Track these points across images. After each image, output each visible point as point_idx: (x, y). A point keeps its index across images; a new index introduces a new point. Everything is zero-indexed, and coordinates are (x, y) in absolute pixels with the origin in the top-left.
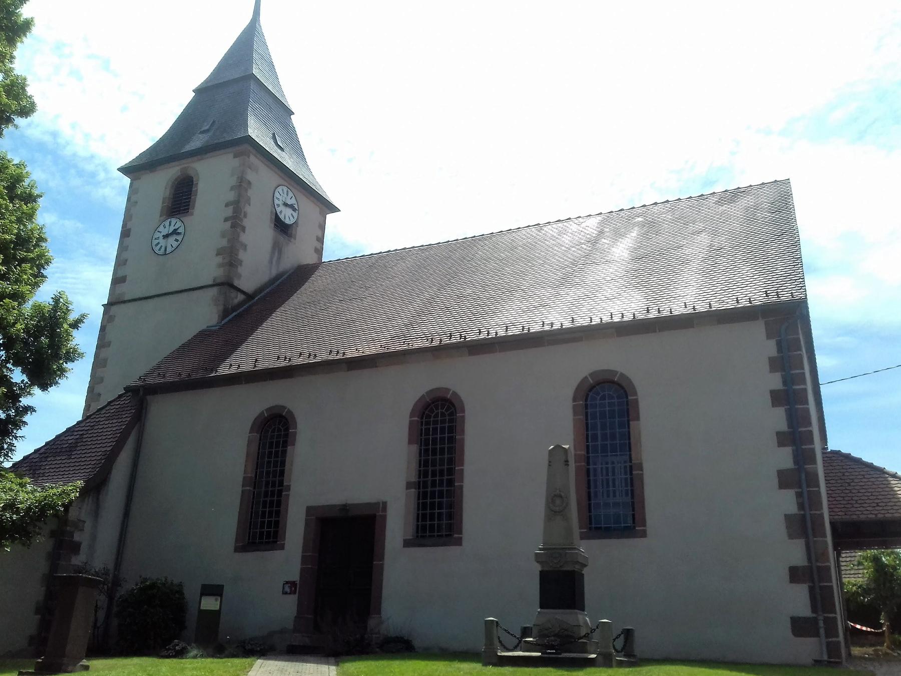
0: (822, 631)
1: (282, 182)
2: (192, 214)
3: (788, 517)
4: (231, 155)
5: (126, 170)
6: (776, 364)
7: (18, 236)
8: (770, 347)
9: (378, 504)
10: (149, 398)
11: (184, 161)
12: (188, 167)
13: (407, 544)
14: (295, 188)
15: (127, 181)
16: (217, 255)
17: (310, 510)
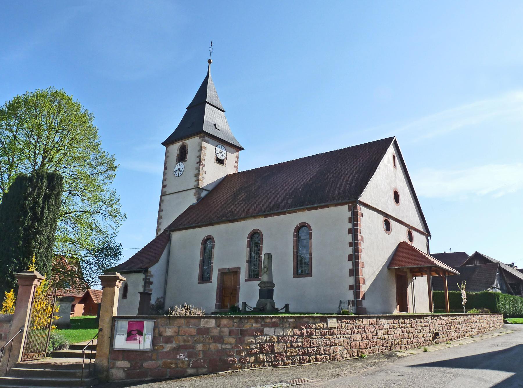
0: (355, 305)
1: (219, 144)
2: (186, 161)
3: (350, 270)
4: (198, 137)
5: (164, 144)
6: (350, 220)
7: (322, 355)
8: (349, 214)
9: (238, 268)
10: (172, 233)
11: (183, 140)
12: (184, 142)
13: (246, 280)
14: (223, 144)
15: (165, 147)
16: (195, 181)
17: (219, 270)
